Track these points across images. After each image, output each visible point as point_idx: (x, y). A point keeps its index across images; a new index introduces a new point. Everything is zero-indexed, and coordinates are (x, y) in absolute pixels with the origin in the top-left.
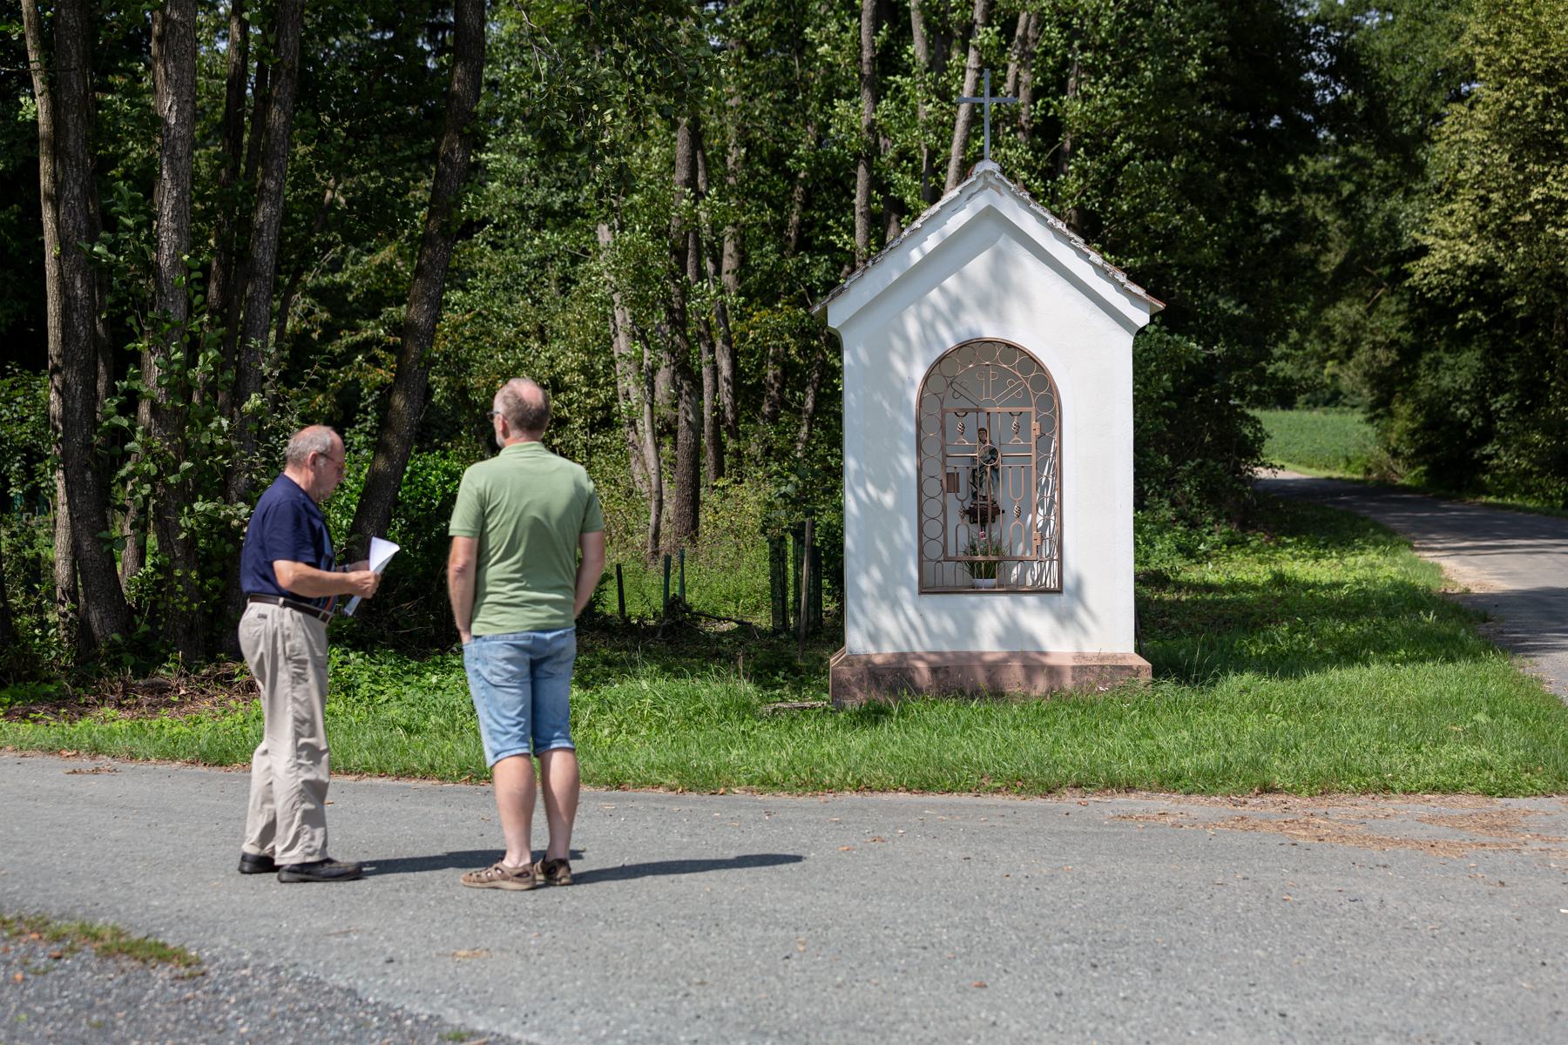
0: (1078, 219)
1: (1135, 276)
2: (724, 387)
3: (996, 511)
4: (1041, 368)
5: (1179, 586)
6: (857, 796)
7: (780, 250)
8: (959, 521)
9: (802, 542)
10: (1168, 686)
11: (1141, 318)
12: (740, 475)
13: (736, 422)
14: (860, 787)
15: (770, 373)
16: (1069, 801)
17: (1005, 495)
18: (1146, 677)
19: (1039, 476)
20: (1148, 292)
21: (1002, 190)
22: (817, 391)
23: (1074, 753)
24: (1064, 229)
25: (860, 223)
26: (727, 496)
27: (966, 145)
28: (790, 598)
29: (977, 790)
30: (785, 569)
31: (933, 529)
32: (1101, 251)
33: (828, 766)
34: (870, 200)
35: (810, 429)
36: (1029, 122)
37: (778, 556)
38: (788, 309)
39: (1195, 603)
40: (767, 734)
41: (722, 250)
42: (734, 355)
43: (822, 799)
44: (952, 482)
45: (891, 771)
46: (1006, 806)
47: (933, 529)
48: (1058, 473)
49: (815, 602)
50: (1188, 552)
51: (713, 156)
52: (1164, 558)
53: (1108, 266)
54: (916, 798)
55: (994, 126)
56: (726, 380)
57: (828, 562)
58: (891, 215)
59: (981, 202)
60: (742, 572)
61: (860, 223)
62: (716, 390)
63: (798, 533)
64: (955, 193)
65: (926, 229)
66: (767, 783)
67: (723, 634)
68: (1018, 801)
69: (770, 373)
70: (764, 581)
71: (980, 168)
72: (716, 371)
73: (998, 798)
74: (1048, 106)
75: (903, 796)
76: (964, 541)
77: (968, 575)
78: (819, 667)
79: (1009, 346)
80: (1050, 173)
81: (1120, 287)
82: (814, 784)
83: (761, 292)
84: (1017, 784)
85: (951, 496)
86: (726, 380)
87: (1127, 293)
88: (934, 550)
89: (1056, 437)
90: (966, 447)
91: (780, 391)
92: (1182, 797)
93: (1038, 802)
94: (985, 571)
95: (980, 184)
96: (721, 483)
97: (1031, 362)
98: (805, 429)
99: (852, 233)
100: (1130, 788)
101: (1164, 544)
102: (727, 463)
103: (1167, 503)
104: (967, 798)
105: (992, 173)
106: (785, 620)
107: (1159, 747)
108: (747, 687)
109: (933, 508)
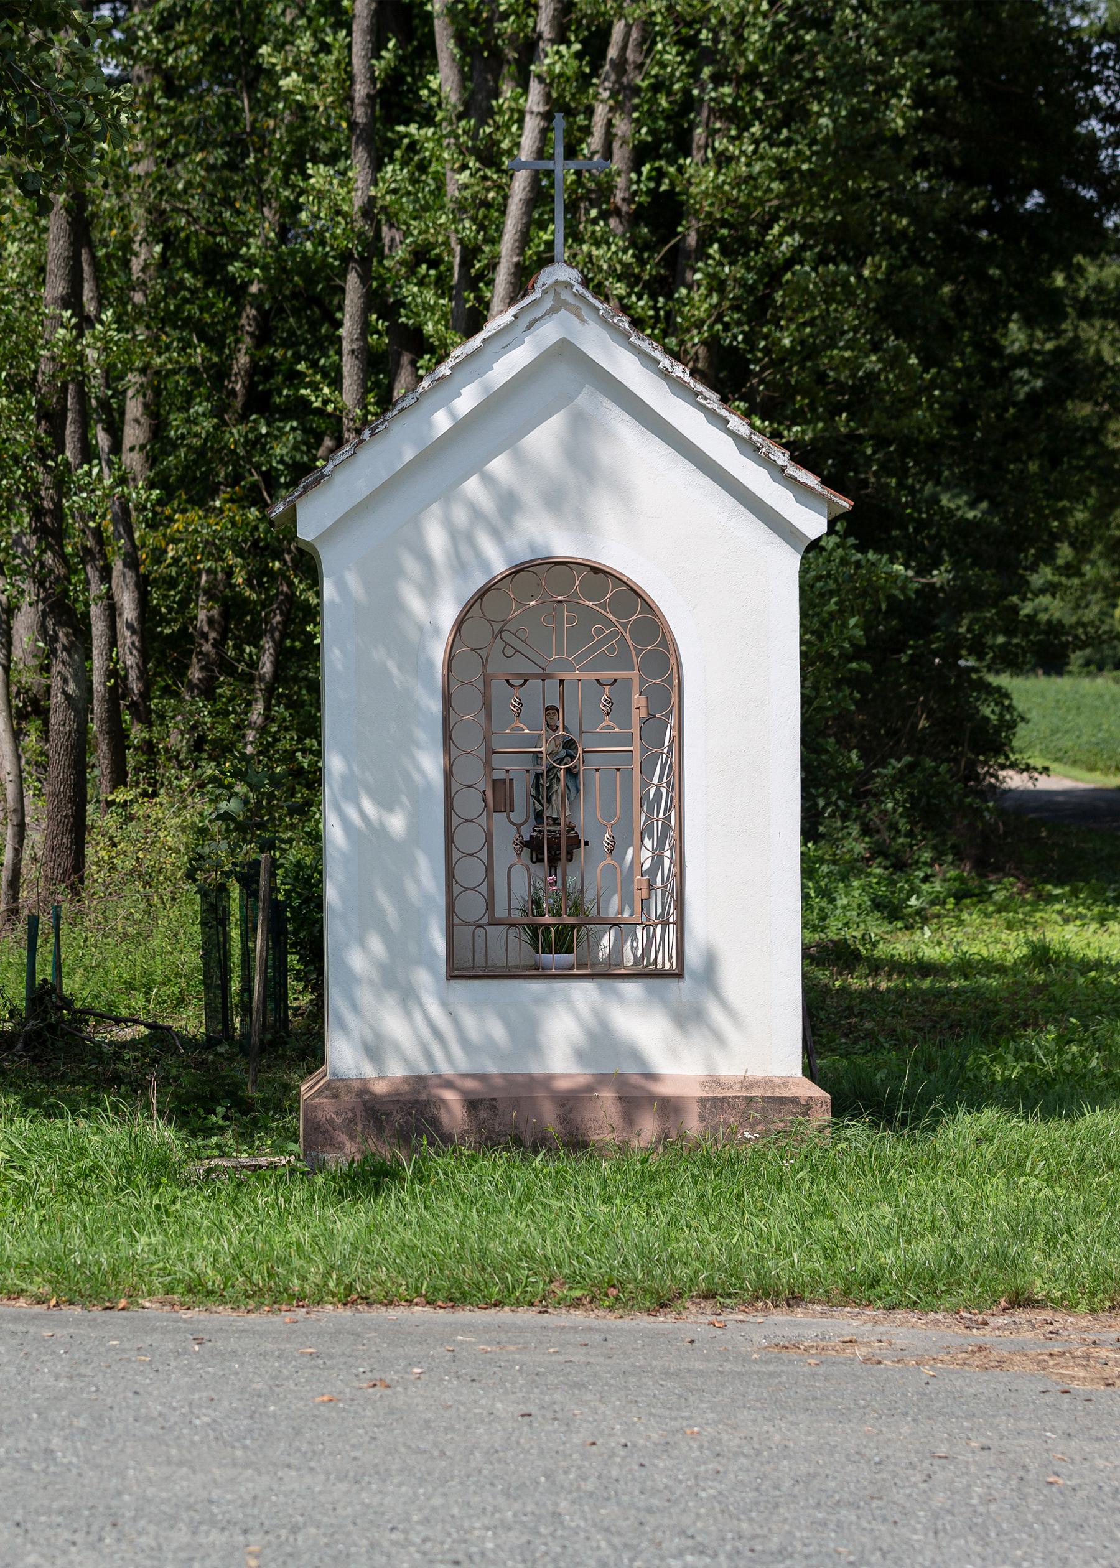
1: (802, 455)
2: (127, 637)
3: (575, 842)
4: (649, 607)
5: (875, 967)
7: (218, 412)
8: (514, 858)
9: (255, 894)
10: (857, 1131)
12: (153, 782)
13: (145, 695)
14: (349, 1297)
15: (202, 615)
16: (696, 1320)
17: (589, 816)
18: (822, 1115)
20: (825, 482)
21: (585, 312)
23: (702, 1241)
24: (687, 378)
25: (350, 368)
26: (130, 818)
27: (525, 239)
28: (235, 986)
29: (542, 1301)
30: (227, 937)
31: (471, 872)
33: (297, 1262)
37: (214, 917)
38: (231, 510)
39: (902, 994)
41: (122, 412)
43: (288, 1317)
44: (501, 795)
45: (401, 1271)
46: (590, 1329)
47: (471, 872)
48: (677, 781)
49: (276, 992)
50: (891, 910)
51: (108, 256)
55: (571, 207)
56: (129, 626)
57: (298, 927)
58: (401, 353)
60: (155, 942)
61: (350, 368)
62: (113, 642)
64: (507, 318)
65: (458, 377)
66: (197, 1290)
67: (123, 1045)
68: (610, 1320)
69: (202, 615)
71: (548, 276)
72: (112, 611)
73: (577, 1316)
74: (660, 175)
75: (420, 1312)
76: (521, 891)
77: (528, 948)
79: (596, 570)
80: (662, 286)
81: (779, 473)
82: (274, 1293)
83: (188, 480)
84: (608, 1292)
85: (499, 818)
87: (792, 483)
88: (473, 907)
91: (219, 644)
92: (880, 1314)
93: (644, 1321)
94: (557, 942)
96: (120, 796)
97: (632, 597)
98: (259, 707)
100: (795, 1299)
101: (851, 897)
102: (131, 763)
103: (855, 830)
104: (526, 1316)
105: (568, 285)
106: (227, 1022)
107: (843, 1232)
109: (470, 838)
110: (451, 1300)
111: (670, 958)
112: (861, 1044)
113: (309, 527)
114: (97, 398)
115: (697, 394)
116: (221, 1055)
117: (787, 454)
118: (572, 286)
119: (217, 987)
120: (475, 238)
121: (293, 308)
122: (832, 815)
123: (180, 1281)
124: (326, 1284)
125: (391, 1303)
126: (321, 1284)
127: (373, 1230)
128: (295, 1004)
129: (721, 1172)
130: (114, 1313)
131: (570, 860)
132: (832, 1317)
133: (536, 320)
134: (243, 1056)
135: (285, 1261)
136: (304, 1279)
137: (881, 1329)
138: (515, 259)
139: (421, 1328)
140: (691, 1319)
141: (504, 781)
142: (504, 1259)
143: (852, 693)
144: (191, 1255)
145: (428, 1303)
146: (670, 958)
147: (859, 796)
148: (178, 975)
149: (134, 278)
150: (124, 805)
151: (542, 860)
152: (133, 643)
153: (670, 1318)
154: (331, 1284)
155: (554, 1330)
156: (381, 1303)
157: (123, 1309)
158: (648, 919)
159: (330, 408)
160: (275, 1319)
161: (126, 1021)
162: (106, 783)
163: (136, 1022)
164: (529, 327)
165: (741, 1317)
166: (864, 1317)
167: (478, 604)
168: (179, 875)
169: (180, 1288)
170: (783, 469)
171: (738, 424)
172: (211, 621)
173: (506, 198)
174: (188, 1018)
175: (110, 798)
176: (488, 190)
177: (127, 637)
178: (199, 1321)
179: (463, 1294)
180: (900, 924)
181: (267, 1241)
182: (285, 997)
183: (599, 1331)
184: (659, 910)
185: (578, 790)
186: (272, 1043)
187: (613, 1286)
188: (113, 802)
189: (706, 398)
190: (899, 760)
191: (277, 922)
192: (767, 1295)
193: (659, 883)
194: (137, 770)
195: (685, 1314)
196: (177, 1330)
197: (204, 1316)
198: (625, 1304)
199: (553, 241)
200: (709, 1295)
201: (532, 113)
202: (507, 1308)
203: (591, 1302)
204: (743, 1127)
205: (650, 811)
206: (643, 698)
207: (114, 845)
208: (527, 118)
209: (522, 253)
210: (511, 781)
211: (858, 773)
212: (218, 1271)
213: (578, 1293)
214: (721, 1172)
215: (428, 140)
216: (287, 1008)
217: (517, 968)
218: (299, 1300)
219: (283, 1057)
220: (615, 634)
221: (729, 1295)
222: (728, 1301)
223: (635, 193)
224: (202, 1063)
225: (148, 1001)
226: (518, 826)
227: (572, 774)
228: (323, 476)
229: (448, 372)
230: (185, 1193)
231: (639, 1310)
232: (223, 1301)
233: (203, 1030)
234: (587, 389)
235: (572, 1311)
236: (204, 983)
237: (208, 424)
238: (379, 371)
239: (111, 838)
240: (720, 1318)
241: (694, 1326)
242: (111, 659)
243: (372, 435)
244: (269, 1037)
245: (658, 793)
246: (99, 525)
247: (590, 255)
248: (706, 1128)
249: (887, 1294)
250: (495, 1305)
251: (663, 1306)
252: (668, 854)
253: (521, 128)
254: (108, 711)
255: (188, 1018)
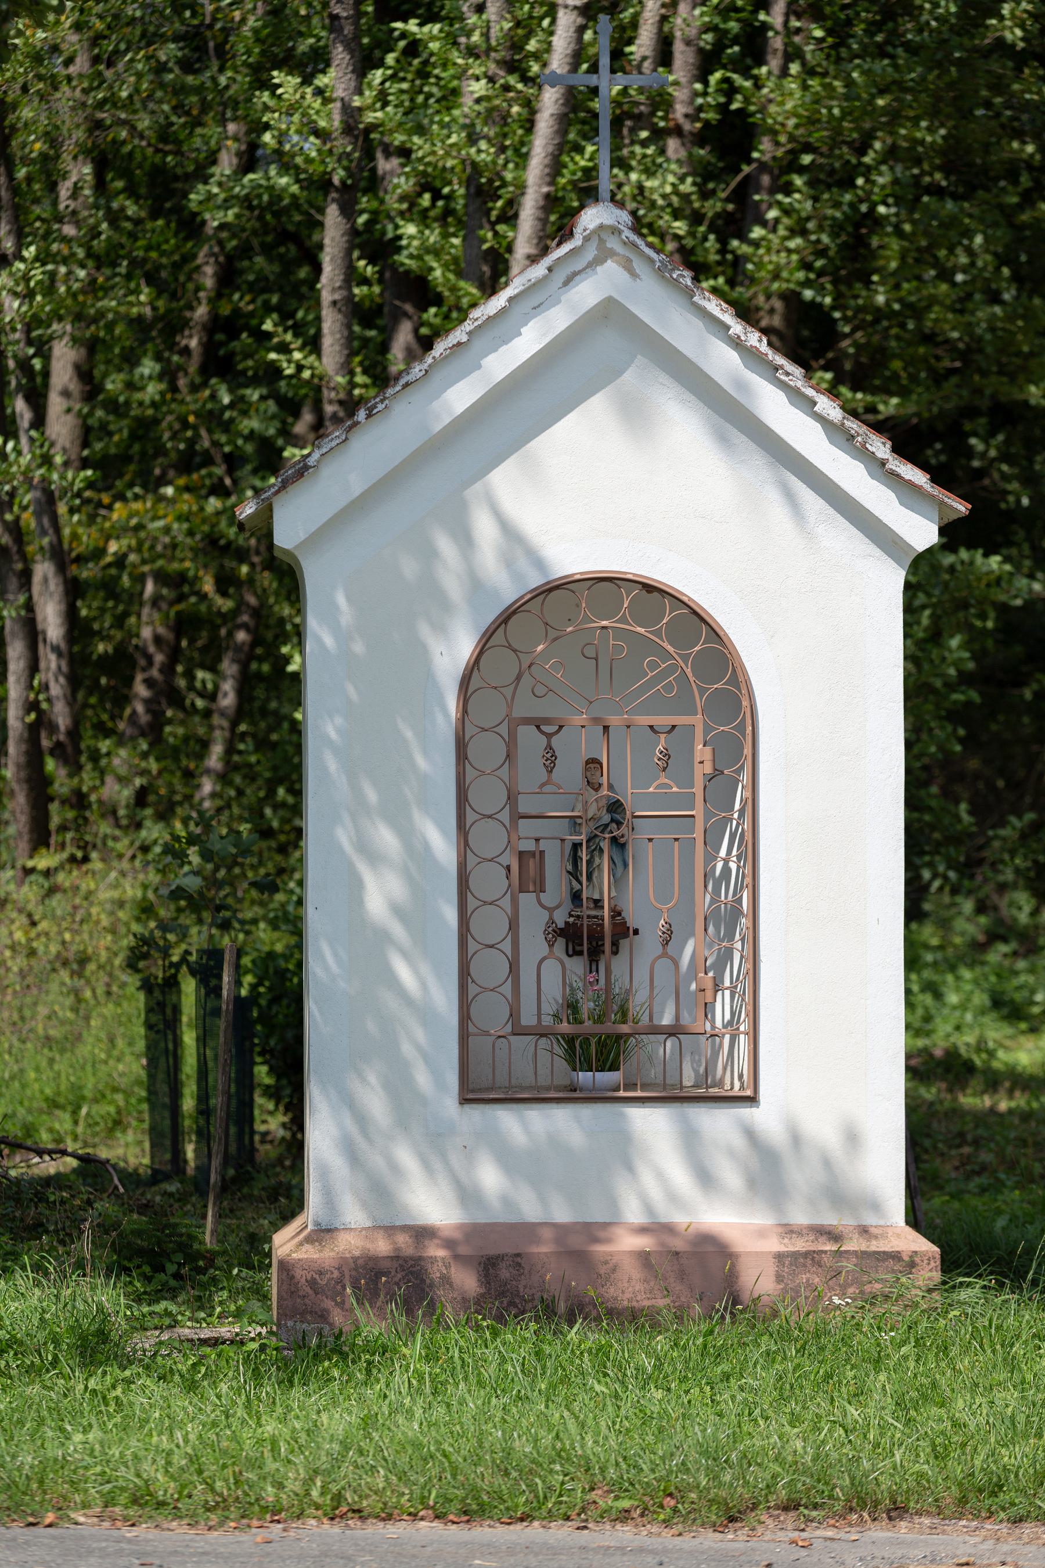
0: (787, 318)
1: (908, 444)
2: (50, 662)
3: (623, 931)
4: (716, 634)
5: (993, 1081)
6: (333, 1530)
7: (169, 375)
8: (545, 949)
9: (217, 991)
10: (971, 1293)
11: (922, 533)
12: (84, 847)
13: (74, 733)
14: (337, 1509)
15: (146, 633)
16: (773, 1537)
17: (641, 894)
18: (930, 1273)
19: (711, 857)
20: (934, 480)
21: (638, 265)
22: (244, 666)
23: (785, 1440)
24: (764, 347)
25: (331, 324)
26: (52, 891)
27: (556, 167)
28: (188, 1104)
29: (581, 1515)
30: (177, 1042)
31: (491, 968)
32: (832, 392)
33: (271, 1466)
34: (351, 276)
35: (230, 750)
36: (692, 117)
37: (162, 1021)
38: (187, 503)
39: (1026, 1116)
40: (147, 1394)
41: (46, 373)
42: (74, 591)
43: (260, 1535)
44: (528, 871)
45: (402, 1476)
46: (641, 1550)
47: (491, 968)
48: (750, 851)
49: (242, 1114)
50: (1010, 1009)
51: (29, 179)
52: (968, 1026)
53: (853, 425)
54: (455, 1533)
55: (617, 123)
56: (56, 649)
57: (268, 1031)
58: (406, 312)
59: (587, 294)
60: (84, 1050)
61: (331, 324)
62: (33, 667)
63: (208, 968)
64: (539, 271)
65: (478, 344)
66: (145, 1502)
67: (48, 1181)
68: (667, 1539)
69: (146, 633)
70: (131, 1066)
71: (591, 218)
72: (33, 633)
73: (625, 1534)
74: (729, 90)
75: (427, 1529)
76: (553, 992)
77: (561, 1065)
78: (255, 1251)
79: (649, 588)
80: (733, 225)
81: (878, 468)
82: (241, 1504)
83: (125, 456)
84: (665, 1502)
85: (527, 900)
86: (56, 649)
87: (893, 480)
88: (493, 1014)
89: (745, 777)
90: (556, 809)
91: (168, 669)
92: (1004, 1528)
93: (709, 1539)
94: (597, 1054)
95: (591, 253)
96: (43, 861)
97: (696, 619)
98: (217, 750)
99: (313, 345)
100: (897, 1511)
101: (964, 990)
102: (55, 821)
103: (968, 906)
104: (561, 1533)
105: (615, 231)
106: (178, 1154)
107: (956, 1424)
108: (106, 1297)
109: (491, 925)
110: (465, 1513)
111: (741, 1076)
112: (977, 1180)
113: (289, 531)
114: (15, 356)
115: (776, 369)
116: (171, 1195)
117: (889, 444)
118: (620, 232)
119: (164, 1105)
120: (494, 162)
121: (263, 245)
122: (941, 889)
123: (123, 1489)
124: (308, 1494)
125: (389, 1517)
126: (301, 1492)
127: (368, 1422)
128: (262, 1128)
129: (803, 1347)
130: (39, 1530)
131: (615, 953)
132: (944, 1532)
133: (575, 274)
134: (191, 1190)
135: (256, 1464)
136: (280, 1486)
137: (1005, 1548)
138: (545, 189)
139: (429, 1549)
140: (768, 1536)
141: (532, 854)
142: (533, 1461)
143: (955, 730)
144: (135, 1456)
145: (437, 1517)
146: (741, 1076)
147: (969, 867)
148: (115, 1090)
149: (62, 207)
150: (47, 873)
151: (580, 953)
152: (59, 668)
153: (743, 1534)
154: (315, 1493)
155: (597, 1550)
156: (377, 1517)
157: (50, 1526)
158: (713, 1027)
159: (306, 374)
160: (244, 1537)
161: (50, 1153)
162: (23, 845)
163: (64, 1153)
164: (568, 281)
165: (830, 1533)
166: (983, 1533)
167: (501, 630)
168: (117, 962)
169: (123, 1499)
170: (883, 463)
171: (826, 405)
172: (158, 640)
173: (533, 112)
174: (127, 1145)
175: (30, 864)
176: (510, 103)
177: (50, 662)
178: (147, 1541)
179: (481, 1505)
180: (1023, 1026)
181: (235, 1438)
182: (251, 1119)
183: (653, 1552)
184: (728, 1017)
185: (625, 865)
186: (234, 1180)
187: (670, 1495)
188: (33, 870)
189: (788, 374)
190: (1020, 817)
191: (246, 1037)
192: (863, 1505)
193: (727, 983)
194: (63, 828)
195: (760, 1530)
196: (120, 1553)
197: (153, 1534)
198: (685, 1518)
199: (595, 168)
200: (790, 1506)
201: (566, 7)
202: (536, 1524)
203: (642, 1515)
204: (831, 1289)
205: (717, 891)
206: (708, 749)
207: (34, 924)
208: (561, 13)
209: (552, 183)
210: (542, 853)
211: (971, 836)
212: (172, 1477)
213: (626, 1504)
214: (803, 1347)
215: (433, 38)
216: (253, 1132)
217: (548, 1089)
218: (274, 1514)
219: (249, 1198)
220: (672, 669)
221: (816, 1506)
222: (814, 1513)
223: (700, 109)
224: (146, 1206)
225: (76, 1123)
226: (551, 910)
227: (619, 844)
228: (306, 467)
229: (465, 338)
230: (127, 1373)
231: (703, 1525)
232: (177, 1514)
233: (146, 1161)
234: (640, 360)
235: (618, 1526)
236: (148, 1100)
237: (153, 390)
238: (371, 330)
239: (30, 916)
240: (804, 1535)
241: (772, 1545)
242: (31, 687)
243: (369, 416)
244: (231, 1172)
245: (726, 870)
246: (18, 519)
247: (641, 188)
248: (785, 1291)
249: (1013, 1504)
250: (522, 1520)
251: (732, 1519)
252: (738, 946)
253: (553, 22)
254: (27, 753)
255: (127, 1145)
